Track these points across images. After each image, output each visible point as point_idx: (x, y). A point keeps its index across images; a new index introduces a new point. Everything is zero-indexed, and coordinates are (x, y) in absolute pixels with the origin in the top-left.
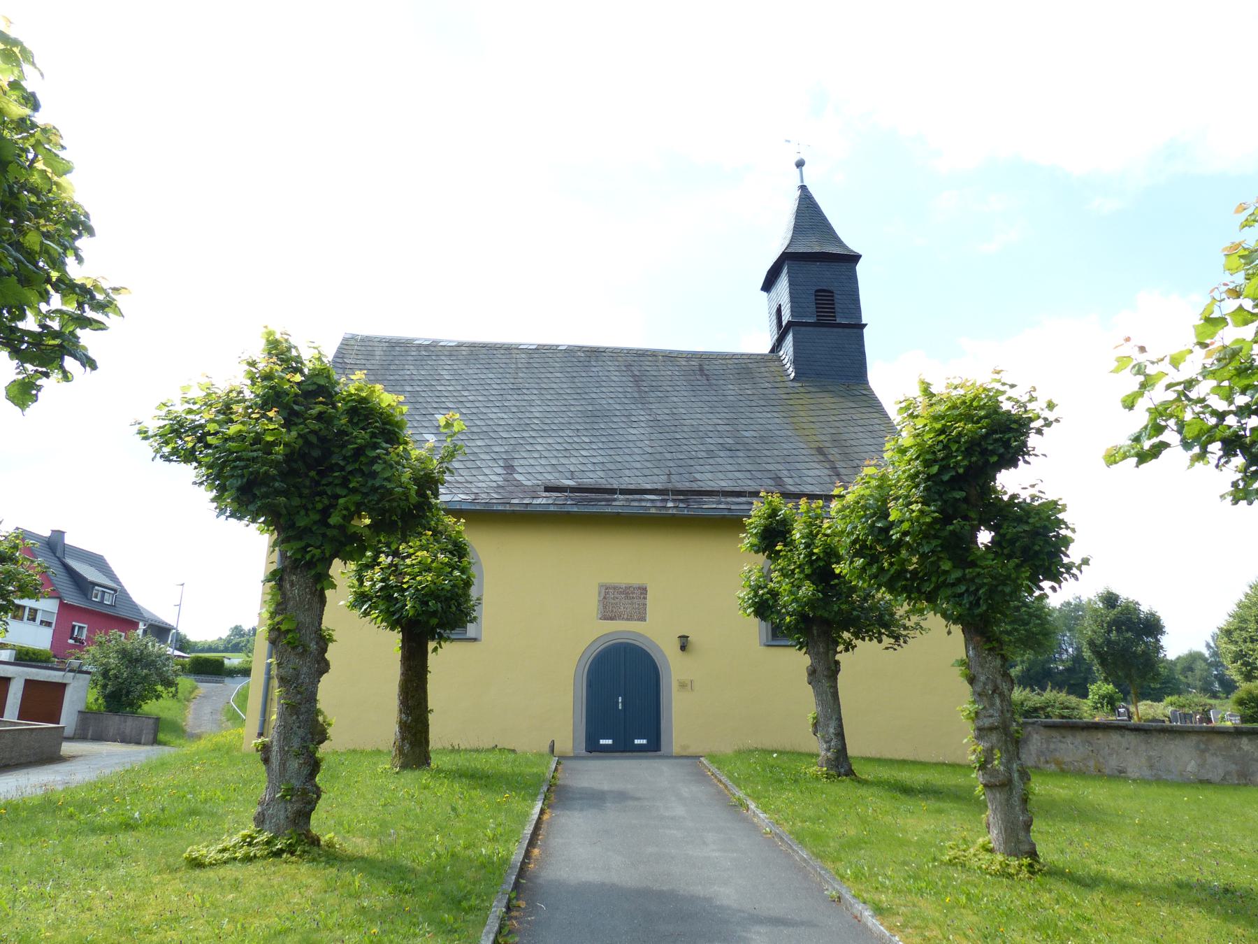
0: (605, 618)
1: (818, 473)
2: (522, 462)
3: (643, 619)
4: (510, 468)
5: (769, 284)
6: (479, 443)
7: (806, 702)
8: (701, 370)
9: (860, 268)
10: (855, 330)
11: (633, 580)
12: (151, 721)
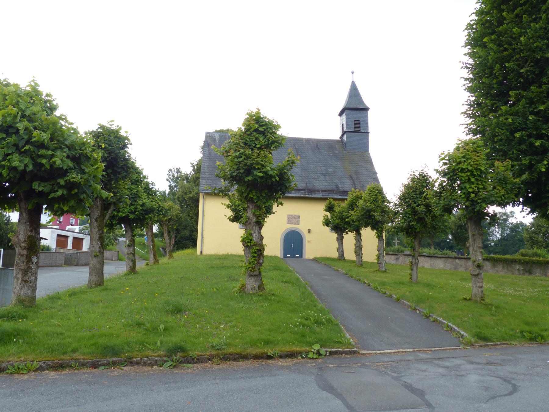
0: (288, 224)
1: (349, 183)
3: (299, 224)
5: (341, 114)
7: (336, 244)
8: (317, 146)
9: (369, 112)
10: (366, 134)
11: (297, 214)
12: (116, 252)
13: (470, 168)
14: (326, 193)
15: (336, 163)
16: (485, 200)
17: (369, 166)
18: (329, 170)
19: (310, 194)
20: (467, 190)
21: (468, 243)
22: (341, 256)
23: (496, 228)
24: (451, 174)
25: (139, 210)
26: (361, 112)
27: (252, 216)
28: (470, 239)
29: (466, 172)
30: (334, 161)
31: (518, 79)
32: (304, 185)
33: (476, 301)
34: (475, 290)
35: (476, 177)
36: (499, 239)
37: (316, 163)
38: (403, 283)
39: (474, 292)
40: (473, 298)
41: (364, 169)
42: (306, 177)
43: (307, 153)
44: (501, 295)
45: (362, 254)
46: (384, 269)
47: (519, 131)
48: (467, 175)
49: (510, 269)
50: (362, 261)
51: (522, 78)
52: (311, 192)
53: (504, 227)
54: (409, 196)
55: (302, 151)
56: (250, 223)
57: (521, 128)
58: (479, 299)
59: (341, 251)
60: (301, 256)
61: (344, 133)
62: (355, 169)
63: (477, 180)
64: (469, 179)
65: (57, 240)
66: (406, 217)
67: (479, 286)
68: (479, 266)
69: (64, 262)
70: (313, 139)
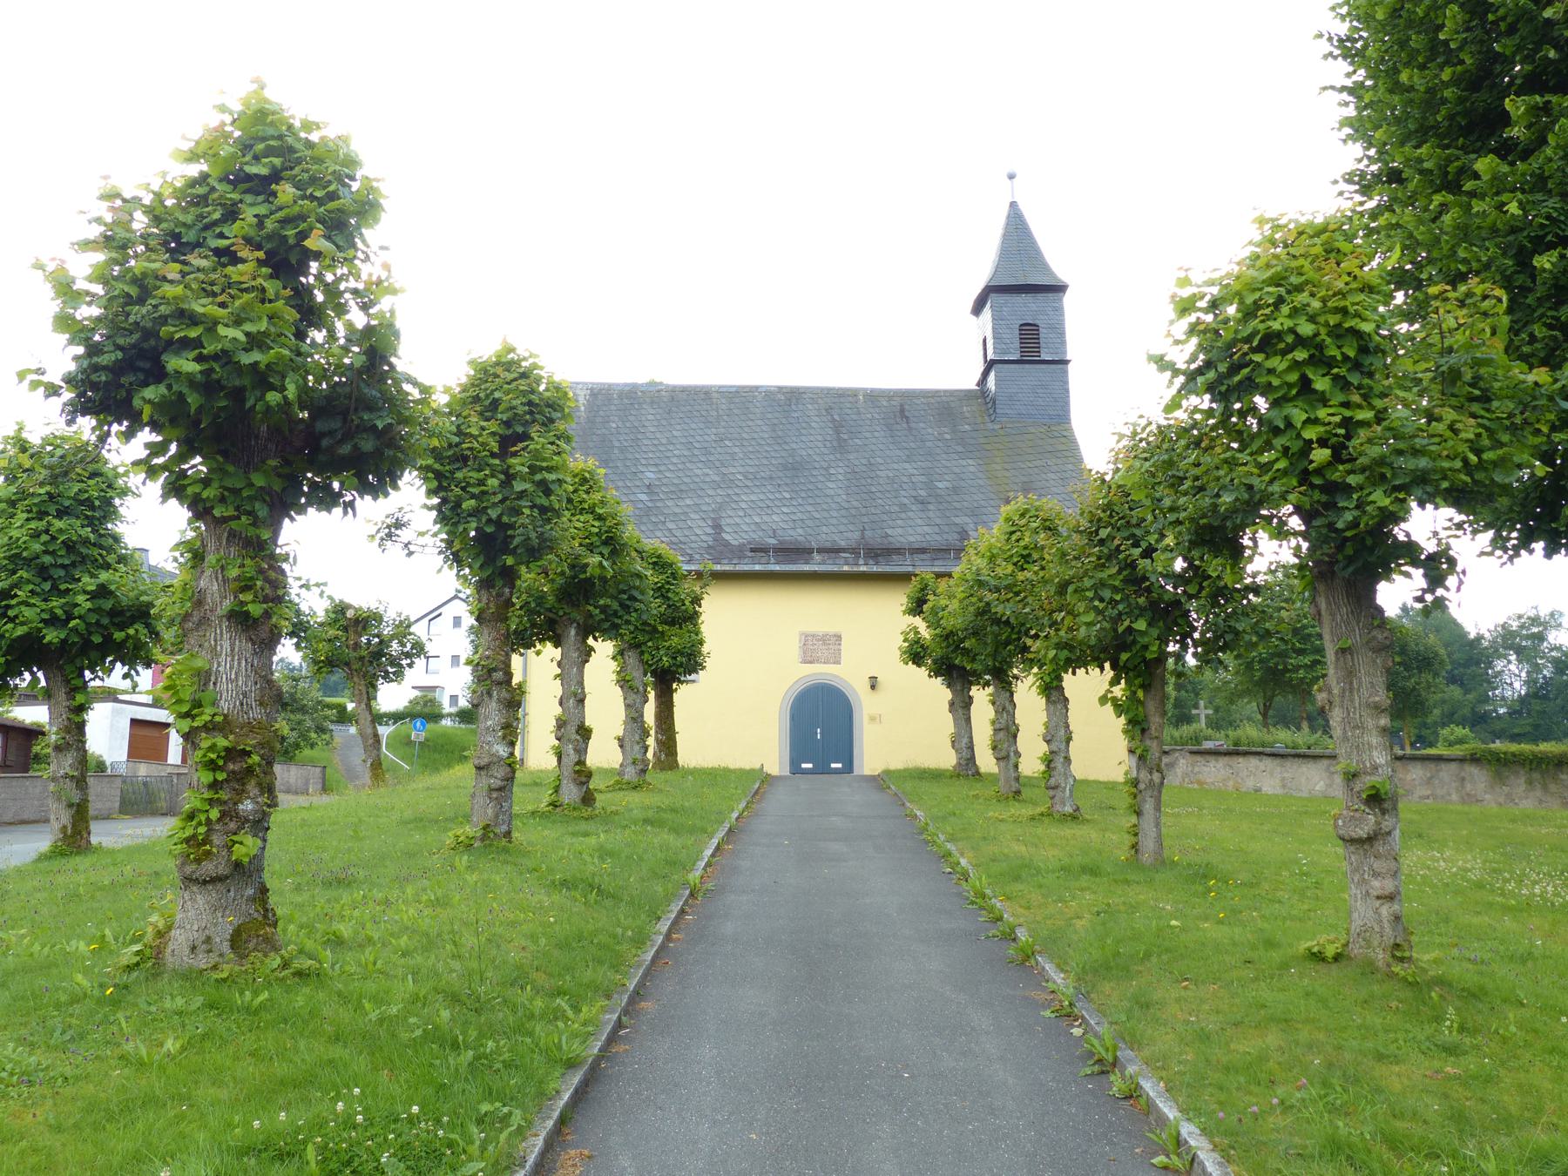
0: (805, 662)
2: (728, 521)
3: (838, 662)
4: (717, 527)
5: (977, 309)
6: (688, 502)
7: (947, 723)
8: (902, 411)
9: (1068, 299)
10: (1060, 366)
13: (1306, 329)
14: (922, 556)
15: (964, 463)
16: (1383, 477)
17: (1070, 466)
18: (940, 485)
19: (871, 562)
20: (1299, 435)
21: (1320, 690)
22: (964, 763)
23: (1510, 662)
24: (1223, 368)
25: (83, 612)
26: (1040, 296)
27: (215, 587)
28: (1331, 671)
29: (1290, 349)
30: (955, 456)
31: (1537, 50)
32: (857, 535)
33: (1369, 968)
34: (1363, 913)
35: (1335, 371)
36: (1520, 695)
37: (896, 466)
38: (1092, 871)
39: (1356, 925)
40: (1356, 950)
41: (1053, 476)
42: (863, 511)
43: (868, 435)
44: (1507, 909)
45: (1018, 754)
46: (1068, 809)
47: (1551, 246)
48: (1296, 365)
49: (1553, 787)
50: (1017, 779)
51: (1555, 47)
52: (877, 556)
53: (1535, 657)
54: (1111, 516)
55: (853, 430)
56: (204, 621)
57: (1557, 235)
58: (1381, 957)
59: (963, 745)
60: (849, 767)
61: (990, 365)
62: (1025, 479)
63: (1342, 383)
64: (1305, 383)
65: (131, 736)
66: (1102, 600)
67: (1379, 892)
68: (1376, 799)
69: (117, 805)
70: (890, 391)
